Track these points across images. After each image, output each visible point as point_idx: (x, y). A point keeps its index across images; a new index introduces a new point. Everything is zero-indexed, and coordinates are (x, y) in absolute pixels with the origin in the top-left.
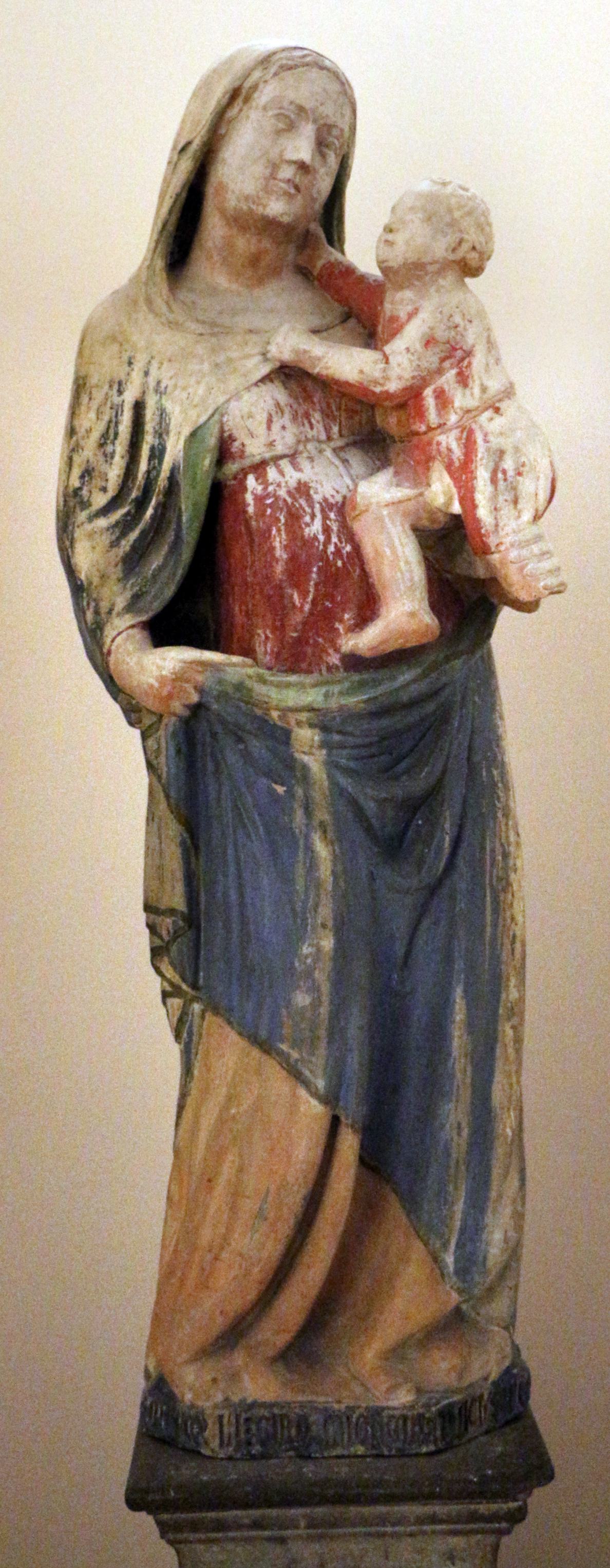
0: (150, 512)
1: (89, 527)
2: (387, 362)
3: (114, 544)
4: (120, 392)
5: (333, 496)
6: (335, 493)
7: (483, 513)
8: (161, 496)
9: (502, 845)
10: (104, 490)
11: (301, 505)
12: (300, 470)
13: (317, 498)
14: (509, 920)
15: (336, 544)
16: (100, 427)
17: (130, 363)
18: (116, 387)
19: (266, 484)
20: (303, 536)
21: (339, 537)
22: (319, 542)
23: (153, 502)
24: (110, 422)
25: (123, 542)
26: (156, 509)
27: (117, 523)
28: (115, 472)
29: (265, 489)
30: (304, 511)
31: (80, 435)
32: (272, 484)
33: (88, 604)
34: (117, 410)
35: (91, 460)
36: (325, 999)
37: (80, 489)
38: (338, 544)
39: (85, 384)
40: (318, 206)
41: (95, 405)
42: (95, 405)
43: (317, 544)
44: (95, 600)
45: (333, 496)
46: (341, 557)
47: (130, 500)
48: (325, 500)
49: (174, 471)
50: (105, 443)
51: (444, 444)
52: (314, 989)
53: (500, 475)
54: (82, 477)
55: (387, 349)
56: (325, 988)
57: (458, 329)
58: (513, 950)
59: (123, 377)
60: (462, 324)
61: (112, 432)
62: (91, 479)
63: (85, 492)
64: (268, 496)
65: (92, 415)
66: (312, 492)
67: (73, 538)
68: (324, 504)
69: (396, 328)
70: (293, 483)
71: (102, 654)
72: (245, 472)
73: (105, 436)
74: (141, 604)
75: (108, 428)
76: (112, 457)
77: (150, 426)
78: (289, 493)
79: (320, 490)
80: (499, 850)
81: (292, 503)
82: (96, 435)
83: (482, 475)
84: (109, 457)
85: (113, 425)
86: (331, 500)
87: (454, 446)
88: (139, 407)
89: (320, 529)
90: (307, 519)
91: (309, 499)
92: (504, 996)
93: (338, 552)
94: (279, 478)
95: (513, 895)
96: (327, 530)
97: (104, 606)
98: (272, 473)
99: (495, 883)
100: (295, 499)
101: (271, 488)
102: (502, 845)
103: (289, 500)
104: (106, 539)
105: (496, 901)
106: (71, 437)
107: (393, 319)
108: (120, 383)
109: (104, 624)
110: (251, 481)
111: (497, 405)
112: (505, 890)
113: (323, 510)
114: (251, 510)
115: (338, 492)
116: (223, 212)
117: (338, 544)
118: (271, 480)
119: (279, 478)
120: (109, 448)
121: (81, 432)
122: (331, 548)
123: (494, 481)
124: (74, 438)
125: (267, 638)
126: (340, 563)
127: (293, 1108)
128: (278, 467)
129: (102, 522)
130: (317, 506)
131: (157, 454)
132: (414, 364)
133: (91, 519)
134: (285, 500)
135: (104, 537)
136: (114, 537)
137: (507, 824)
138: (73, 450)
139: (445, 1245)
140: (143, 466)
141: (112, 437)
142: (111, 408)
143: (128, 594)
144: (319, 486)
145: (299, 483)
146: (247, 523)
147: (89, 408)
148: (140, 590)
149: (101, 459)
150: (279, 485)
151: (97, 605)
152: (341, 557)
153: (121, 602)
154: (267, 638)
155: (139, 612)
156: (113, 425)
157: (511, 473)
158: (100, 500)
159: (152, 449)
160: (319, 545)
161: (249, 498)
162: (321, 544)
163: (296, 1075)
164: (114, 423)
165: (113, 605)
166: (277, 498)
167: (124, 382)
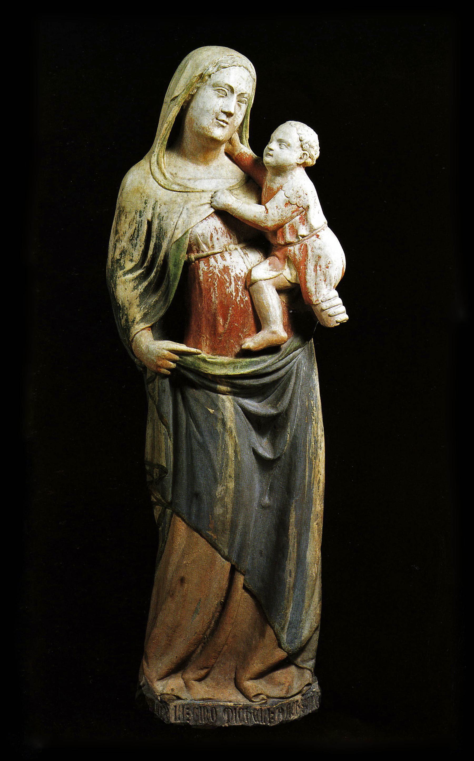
0: (153, 274)
1: (123, 278)
2: (267, 213)
3: (135, 288)
4: (140, 216)
5: (240, 273)
6: (240, 272)
7: (311, 286)
8: (159, 268)
9: (315, 437)
10: (131, 260)
11: (224, 278)
12: (225, 260)
13: (233, 274)
14: (317, 473)
15: (240, 296)
16: (132, 231)
17: (146, 203)
18: (138, 214)
19: (209, 266)
20: (225, 293)
21: (242, 294)
22: (233, 296)
23: (155, 270)
24: (135, 229)
25: (140, 287)
26: (156, 273)
27: (136, 278)
28: (137, 255)
29: (208, 269)
30: (226, 281)
31: (120, 234)
32: (211, 266)
33: (123, 316)
34: (140, 224)
35: (125, 247)
36: (230, 511)
37: (120, 260)
38: (242, 296)
39: (124, 210)
40: (237, 128)
41: (128, 220)
42: (128, 220)
43: (232, 297)
44: (126, 315)
45: (240, 273)
46: (243, 303)
47: (143, 267)
48: (236, 275)
49: (166, 256)
50: (133, 239)
51: (293, 251)
52: (224, 506)
53: (318, 268)
54: (121, 254)
55: (268, 205)
56: (230, 506)
57: (301, 198)
58: (319, 486)
59: (142, 209)
60: (302, 195)
61: (136, 233)
62: (125, 255)
63: (122, 261)
64: (210, 272)
65: (127, 226)
66: (230, 271)
67: (116, 283)
68: (235, 277)
69: (272, 194)
70: (221, 267)
71: (129, 340)
72: (198, 259)
73: (133, 236)
74: (148, 317)
75: (134, 232)
76: (136, 246)
77: (154, 234)
78: (219, 271)
79: (234, 270)
80: (313, 440)
81: (221, 277)
82: (128, 235)
83: (311, 267)
84: (135, 246)
85: (136, 231)
86: (239, 275)
87: (297, 252)
88: (150, 224)
89: (234, 290)
90: (228, 284)
91: (229, 275)
92: (313, 509)
93: (242, 300)
94: (215, 264)
95: (319, 461)
96: (237, 290)
97: (131, 318)
98: (212, 260)
99: (311, 456)
100: (222, 274)
101: (211, 269)
102: (315, 437)
103: (219, 275)
104: (131, 285)
105: (311, 463)
106: (116, 235)
107: (270, 189)
108: (140, 212)
109: (130, 327)
110: (202, 265)
111: (318, 234)
112: (315, 458)
113: (235, 280)
114: (201, 278)
115: (242, 271)
116: (191, 132)
117: (242, 296)
118: (211, 265)
119: (215, 264)
120: (135, 242)
121: (121, 233)
122: (239, 299)
123: (315, 271)
124: (118, 236)
125: (207, 338)
126: (242, 306)
127: (213, 563)
128: (214, 258)
129: (130, 276)
130: (232, 278)
131: (158, 247)
132: (280, 214)
133: (125, 274)
134: (217, 275)
135: (131, 284)
136: (135, 284)
137: (317, 427)
138: (117, 241)
139: (283, 629)
140: (150, 253)
141: (136, 237)
142: (136, 223)
143: (142, 313)
144: (233, 268)
145: (224, 267)
146: (199, 283)
147: (125, 222)
148: (148, 311)
149: (131, 246)
150: (215, 268)
151: (127, 317)
152: (243, 303)
153: (138, 317)
154: (207, 338)
155: (147, 322)
156: (136, 231)
157: (323, 267)
158: (129, 265)
159: (155, 245)
160: (233, 297)
161: (201, 272)
162: (234, 297)
163: (214, 546)
164: (137, 230)
165: (135, 318)
166: (214, 274)
167: (142, 211)
